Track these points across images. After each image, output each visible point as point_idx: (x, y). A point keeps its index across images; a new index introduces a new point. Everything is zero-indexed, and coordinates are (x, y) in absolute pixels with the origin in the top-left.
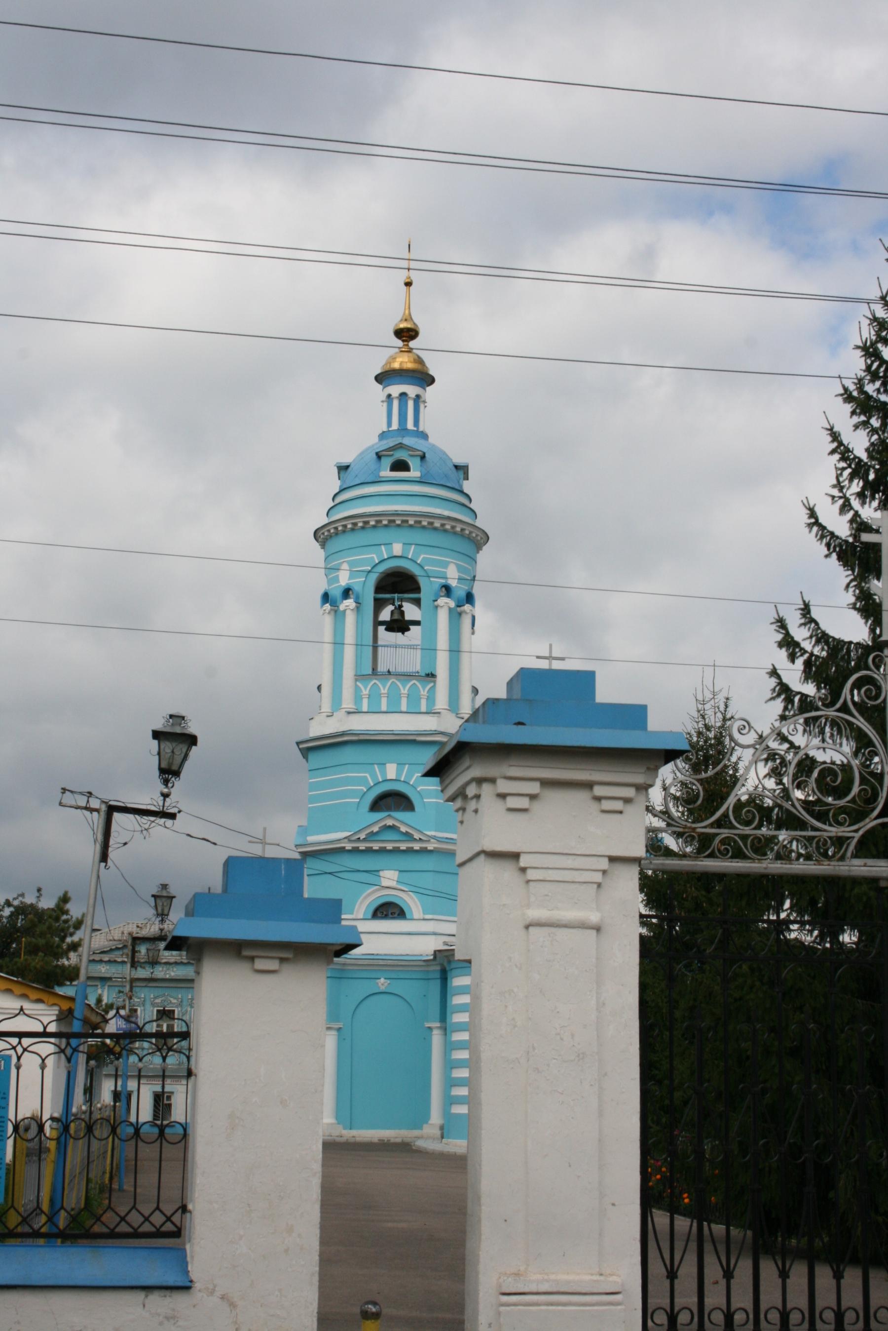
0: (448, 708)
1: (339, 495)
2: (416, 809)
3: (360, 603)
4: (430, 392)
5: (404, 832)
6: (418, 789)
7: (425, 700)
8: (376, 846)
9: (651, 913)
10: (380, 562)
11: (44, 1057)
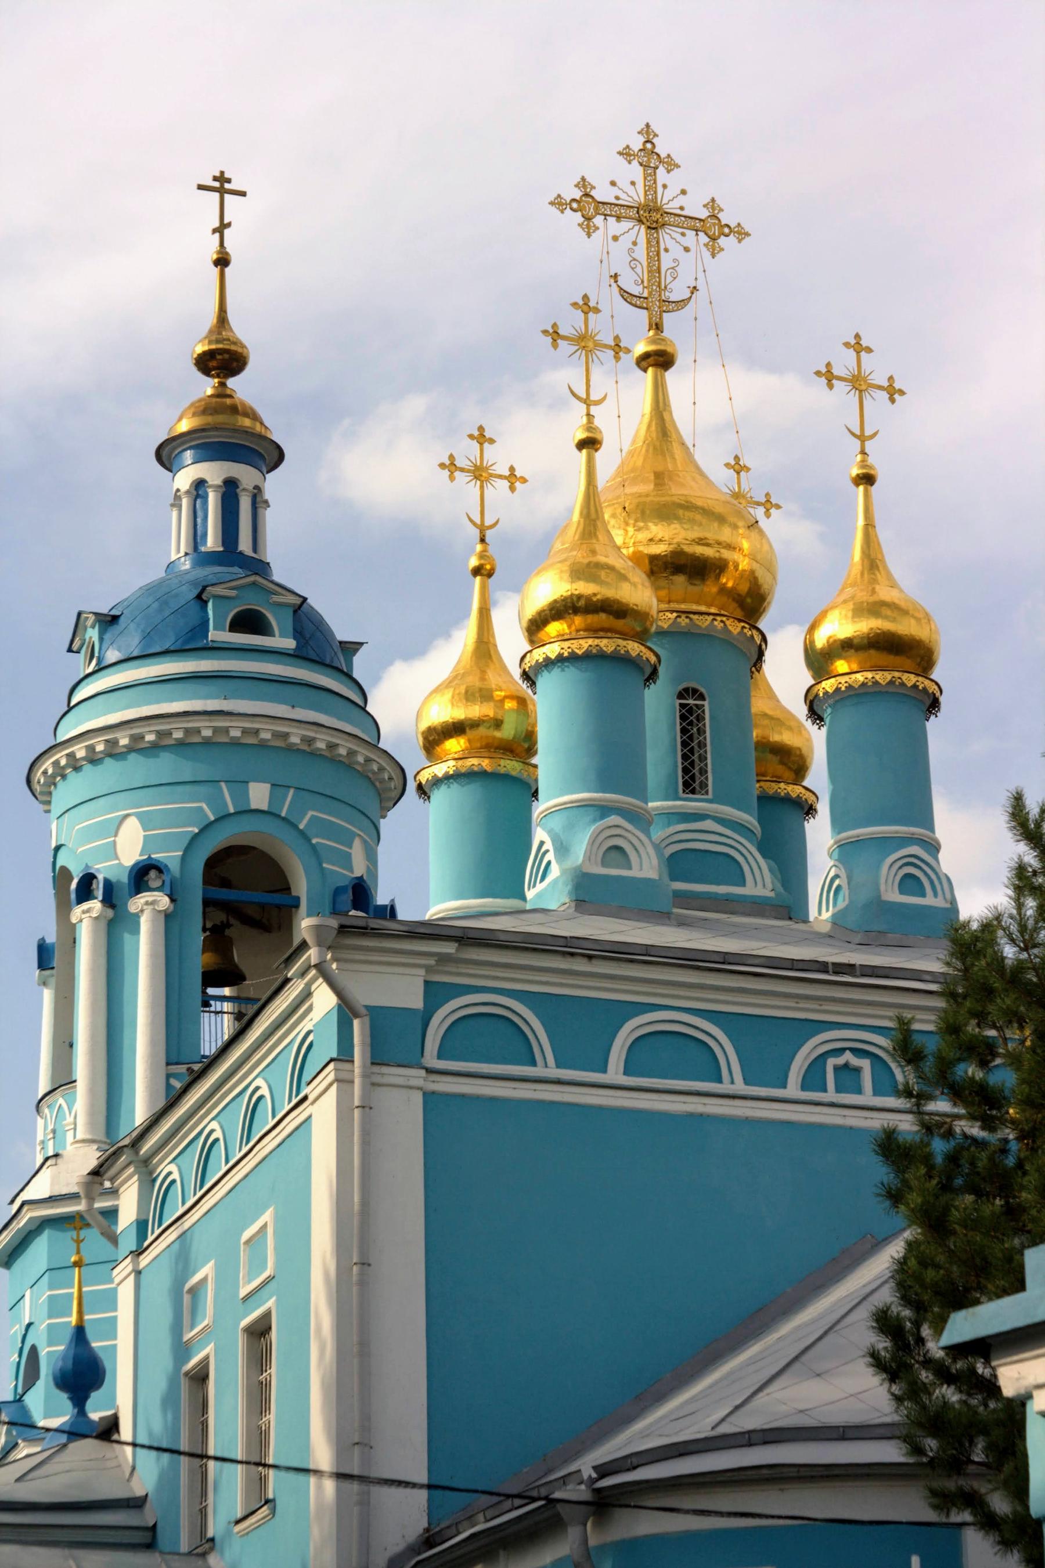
1: (170, 654)
4: (274, 485)
6: (292, 791)
9: (956, 1110)
11: (227, 196)
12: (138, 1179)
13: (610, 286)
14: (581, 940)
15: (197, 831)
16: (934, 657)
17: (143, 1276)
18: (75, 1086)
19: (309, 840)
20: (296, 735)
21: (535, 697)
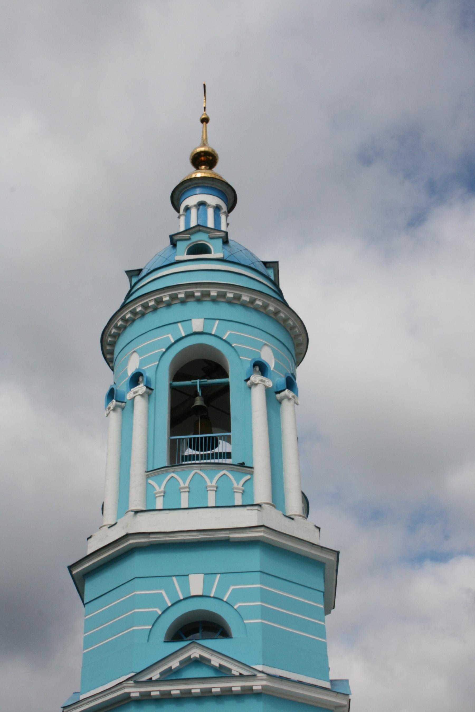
0: (271, 502)
2: (233, 635)
3: (152, 389)
5: (217, 665)
7: (240, 495)
8: (175, 689)
10: (177, 341)
14: (207, 193)
16: (217, 161)
20: (127, 313)
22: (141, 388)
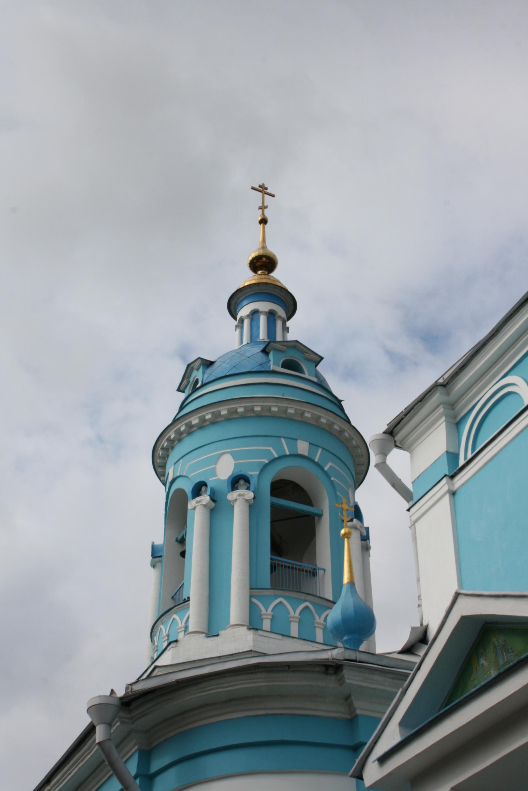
6: (320, 450)
7: (297, 624)
12: (446, 420)
13: (313, 647)
15: (267, 462)
17: (457, 496)
18: (189, 604)
19: (329, 477)
21: (273, 572)
22: (205, 498)
